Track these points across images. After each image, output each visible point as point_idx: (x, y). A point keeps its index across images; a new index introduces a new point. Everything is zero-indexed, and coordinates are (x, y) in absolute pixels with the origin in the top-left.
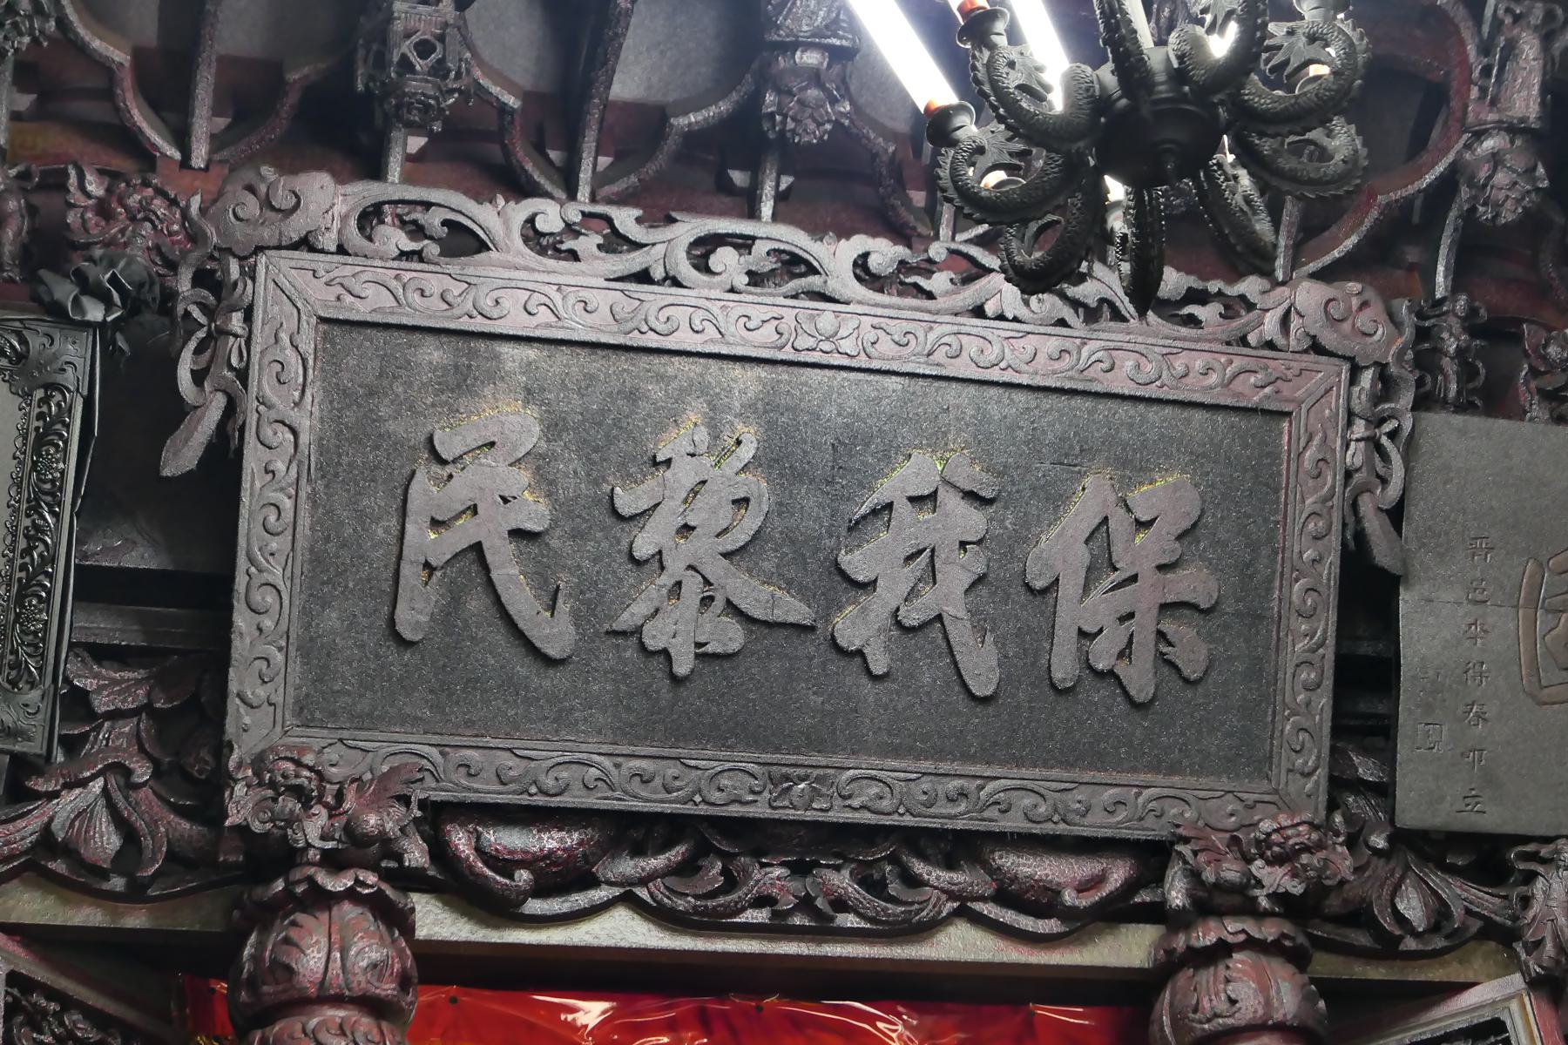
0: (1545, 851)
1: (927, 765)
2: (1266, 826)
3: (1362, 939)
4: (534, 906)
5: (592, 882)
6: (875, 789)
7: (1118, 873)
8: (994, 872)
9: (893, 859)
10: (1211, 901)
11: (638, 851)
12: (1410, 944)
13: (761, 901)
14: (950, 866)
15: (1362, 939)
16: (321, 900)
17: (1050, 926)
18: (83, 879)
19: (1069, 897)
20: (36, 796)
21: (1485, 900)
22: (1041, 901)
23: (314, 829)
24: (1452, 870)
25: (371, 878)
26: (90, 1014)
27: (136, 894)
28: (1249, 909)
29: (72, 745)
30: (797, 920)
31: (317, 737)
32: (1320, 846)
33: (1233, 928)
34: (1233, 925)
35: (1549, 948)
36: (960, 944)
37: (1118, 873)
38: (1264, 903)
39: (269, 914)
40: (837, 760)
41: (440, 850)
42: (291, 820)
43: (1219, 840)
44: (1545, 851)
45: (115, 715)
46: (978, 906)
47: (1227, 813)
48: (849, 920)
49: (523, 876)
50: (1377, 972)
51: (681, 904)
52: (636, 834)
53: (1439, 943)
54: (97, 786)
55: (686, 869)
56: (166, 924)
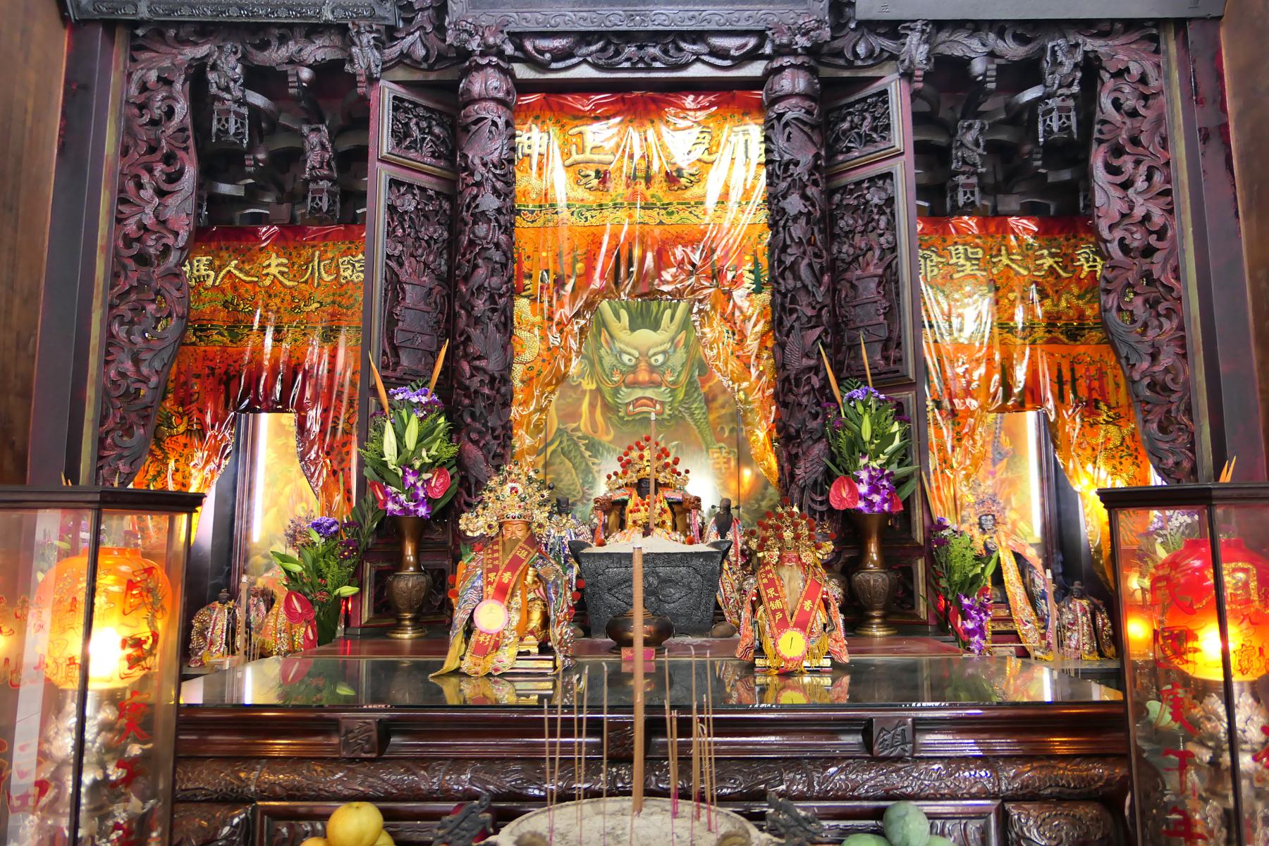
0: (912, 25)
1: (681, 7)
2: (801, 22)
3: (842, 62)
4: (554, 65)
5: (572, 56)
6: (664, 17)
7: (752, 42)
8: (708, 44)
9: (674, 42)
10: (780, 51)
11: (589, 44)
12: (859, 63)
13: (628, 60)
14: (694, 43)
15: (842, 62)
16: (480, 68)
17: (728, 63)
18: (415, 65)
19: (732, 52)
20: (397, 39)
21: (889, 44)
22: (722, 54)
23: (474, 45)
24: (879, 35)
25: (495, 59)
26: (426, 108)
27: (431, 69)
28: (794, 53)
29: (408, 21)
30: (640, 65)
31: (477, 13)
32: (818, 28)
33: (786, 61)
34: (786, 59)
35: (907, 63)
36: (698, 71)
37: (752, 42)
38: (800, 50)
39: (466, 73)
40: (650, 8)
41: (519, 47)
42: (466, 41)
43: (785, 28)
44: (912, 25)
45: (421, 10)
46: (703, 57)
47: (790, 18)
48: (657, 65)
49: (548, 56)
50: (846, 74)
51: (601, 62)
52: (589, 38)
53: (870, 62)
54: (417, 34)
55: (603, 50)
56: (442, 78)
